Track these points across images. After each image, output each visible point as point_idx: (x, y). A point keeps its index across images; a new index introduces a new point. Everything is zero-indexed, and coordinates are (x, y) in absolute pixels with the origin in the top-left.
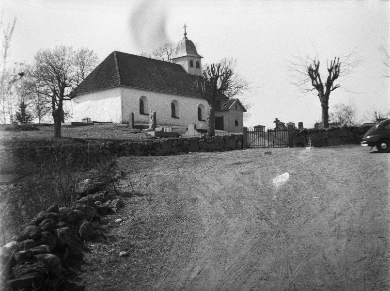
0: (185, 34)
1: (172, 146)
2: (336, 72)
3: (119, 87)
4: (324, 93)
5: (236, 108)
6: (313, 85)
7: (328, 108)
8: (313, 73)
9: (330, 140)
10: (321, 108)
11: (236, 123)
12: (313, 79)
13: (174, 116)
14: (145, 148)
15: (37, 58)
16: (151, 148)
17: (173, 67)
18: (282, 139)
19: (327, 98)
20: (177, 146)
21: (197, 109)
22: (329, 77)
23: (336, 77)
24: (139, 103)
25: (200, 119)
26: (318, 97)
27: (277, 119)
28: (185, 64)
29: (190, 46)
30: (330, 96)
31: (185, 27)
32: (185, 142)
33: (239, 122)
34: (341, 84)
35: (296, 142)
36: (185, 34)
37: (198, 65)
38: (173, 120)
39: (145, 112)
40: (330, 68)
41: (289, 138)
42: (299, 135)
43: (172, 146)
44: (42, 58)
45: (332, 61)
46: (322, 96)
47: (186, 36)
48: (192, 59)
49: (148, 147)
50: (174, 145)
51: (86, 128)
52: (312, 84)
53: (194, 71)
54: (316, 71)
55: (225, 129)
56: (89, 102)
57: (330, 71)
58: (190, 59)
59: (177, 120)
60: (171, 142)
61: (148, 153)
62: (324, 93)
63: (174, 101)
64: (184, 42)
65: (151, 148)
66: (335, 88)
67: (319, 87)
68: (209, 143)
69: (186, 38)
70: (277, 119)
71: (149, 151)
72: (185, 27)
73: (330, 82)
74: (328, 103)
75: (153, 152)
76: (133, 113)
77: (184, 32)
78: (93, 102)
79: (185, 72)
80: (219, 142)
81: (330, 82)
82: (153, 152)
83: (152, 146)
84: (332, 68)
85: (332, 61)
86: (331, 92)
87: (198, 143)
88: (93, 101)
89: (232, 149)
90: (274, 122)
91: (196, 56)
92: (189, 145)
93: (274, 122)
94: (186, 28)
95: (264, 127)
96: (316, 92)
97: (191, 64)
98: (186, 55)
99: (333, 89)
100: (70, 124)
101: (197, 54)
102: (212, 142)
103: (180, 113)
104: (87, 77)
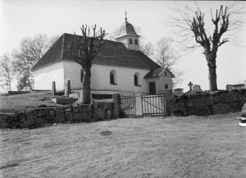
0: (126, 19)
1: (38, 117)
2: (224, 22)
3: (62, 61)
4: (211, 50)
5: (166, 75)
6: (197, 41)
7: (215, 67)
8: (198, 28)
9: (215, 107)
10: (207, 68)
11: (166, 86)
12: (197, 34)
13: (112, 81)
14: (10, 120)
15: (22, 44)
16: (16, 119)
17: (116, 45)
18: (158, 107)
19: (214, 56)
20: (42, 117)
21: (133, 78)
22: (216, 30)
23: (223, 30)
24: (109, 76)
25: (136, 84)
26: (204, 56)
27: (190, 83)
28: (125, 42)
29: (129, 27)
30: (218, 53)
31: (126, 13)
32: (51, 112)
33: (169, 86)
34: (230, 38)
35: (174, 110)
36: (126, 19)
37: (137, 42)
38: (112, 87)
39: (139, 84)
40: (215, 20)
41: (167, 105)
42: (177, 101)
43: (38, 117)
44: (26, 44)
45: (217, 10)
46: (208, 54)
47: (127, 20)
48: (132, 38)
49: (13, 118)
50: (39, 115)
51: (19, 95)
52: (196, 40)
53: (133, 47)
54: (202, 26)
55: (157, 93)
56: (43, 74)
57: (216, 23)
58: (129, 38)
59: (115, 86)
60: (35, 112)
61: (13, 125)
62: (211, 50)
63: (136, 73)
64: (125, 25)
65: (16, 119)
66: (223, 43)
67: (205, 43)
68: (76, 113)
69: (127, 22)
70: (190, 83)
71: (14, 123)
72: (126, 13)
73: (217, 36)
74: (215, 61)
75: (18, 123)
76: (54, 82)
77: (125, 18)
78: (46, 74)
79: (125, 47)
80: (87, 112)
81: (217, 36)
82: (18, 123)
83: (18, 117)
84: (218, 19)
85: (217, 10)
86: (219, 48)
87: (64, 113)
88: (46, 73)
89: (100, 120)
90: (189, 85)
91: (135, 35)
92: (55, 115)
93: (189, 85)
94: (127, 14)
95: (183, 89)
96: (202, 49)
97: (131, 42)
98: (126, 34)
99: (221, 44)
100: (7, 93)
101: (135, 33)
102: (79, 112)
103: (117, 80)
104: (43, 56)
